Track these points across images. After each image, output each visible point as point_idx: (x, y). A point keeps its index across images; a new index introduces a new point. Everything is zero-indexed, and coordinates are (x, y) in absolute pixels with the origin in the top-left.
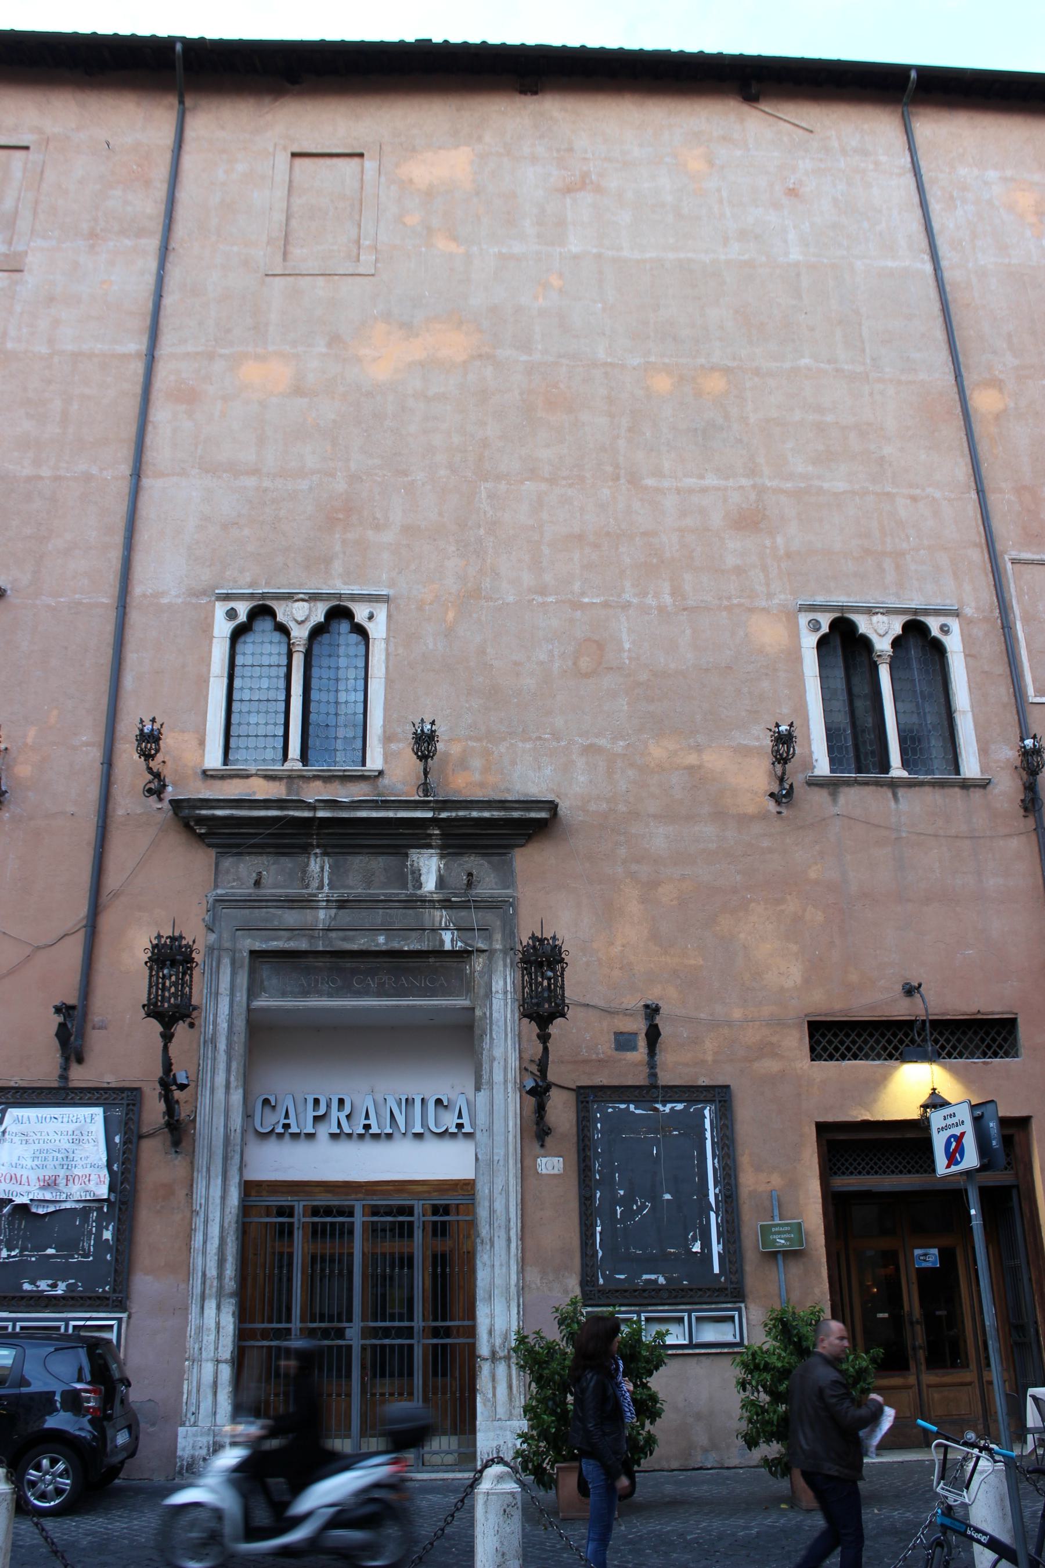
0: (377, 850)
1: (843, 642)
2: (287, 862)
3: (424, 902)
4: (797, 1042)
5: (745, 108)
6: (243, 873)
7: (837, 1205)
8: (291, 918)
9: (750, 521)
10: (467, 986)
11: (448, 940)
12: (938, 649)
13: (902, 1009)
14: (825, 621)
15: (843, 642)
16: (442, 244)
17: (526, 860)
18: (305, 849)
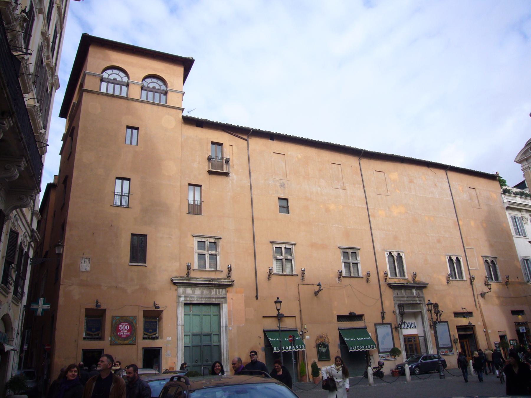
0: (409, 289)
1: (451, 260)
2: (400, 291)
3: (414, 297)
4: (453, 315)
5: (427, 168)
6: (397, 291)
7: (459, 335)
8: (402, 299)
9: (439, 241)
10: (420, 308)
11: (418, 302)
12: (401, 257)
13: (462, 311)
14: (388, 253)
15: (451, 260)
16: (398, 191)
17: (424, 291)
18: (402, 289)
